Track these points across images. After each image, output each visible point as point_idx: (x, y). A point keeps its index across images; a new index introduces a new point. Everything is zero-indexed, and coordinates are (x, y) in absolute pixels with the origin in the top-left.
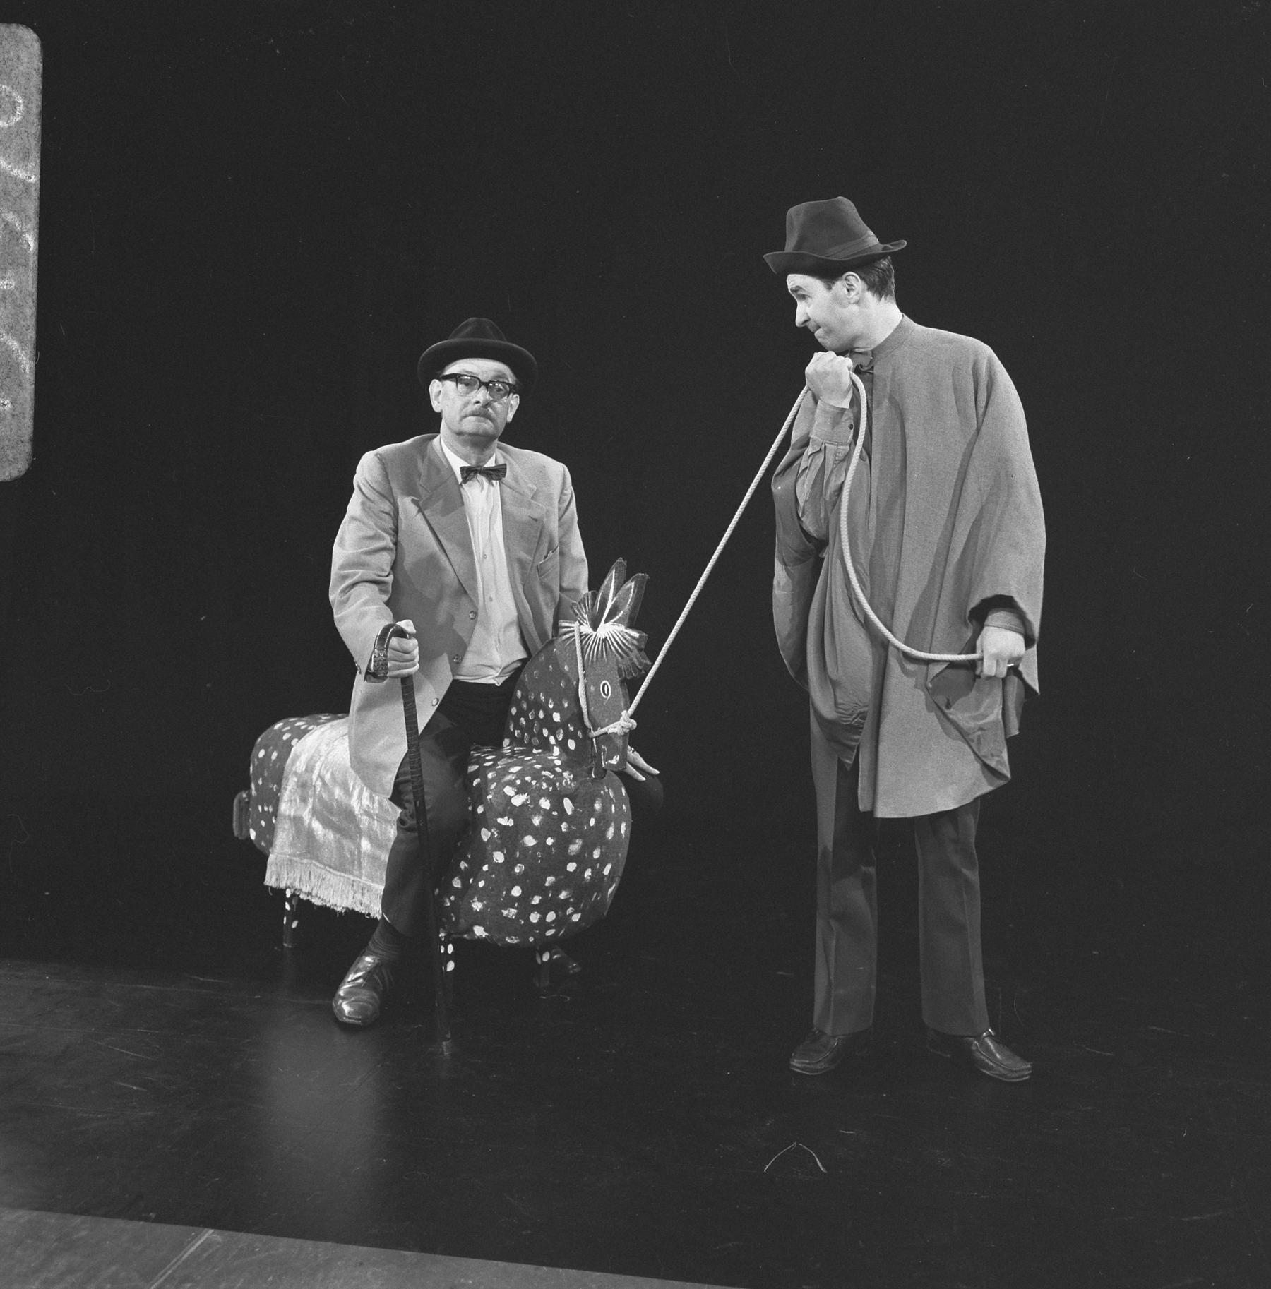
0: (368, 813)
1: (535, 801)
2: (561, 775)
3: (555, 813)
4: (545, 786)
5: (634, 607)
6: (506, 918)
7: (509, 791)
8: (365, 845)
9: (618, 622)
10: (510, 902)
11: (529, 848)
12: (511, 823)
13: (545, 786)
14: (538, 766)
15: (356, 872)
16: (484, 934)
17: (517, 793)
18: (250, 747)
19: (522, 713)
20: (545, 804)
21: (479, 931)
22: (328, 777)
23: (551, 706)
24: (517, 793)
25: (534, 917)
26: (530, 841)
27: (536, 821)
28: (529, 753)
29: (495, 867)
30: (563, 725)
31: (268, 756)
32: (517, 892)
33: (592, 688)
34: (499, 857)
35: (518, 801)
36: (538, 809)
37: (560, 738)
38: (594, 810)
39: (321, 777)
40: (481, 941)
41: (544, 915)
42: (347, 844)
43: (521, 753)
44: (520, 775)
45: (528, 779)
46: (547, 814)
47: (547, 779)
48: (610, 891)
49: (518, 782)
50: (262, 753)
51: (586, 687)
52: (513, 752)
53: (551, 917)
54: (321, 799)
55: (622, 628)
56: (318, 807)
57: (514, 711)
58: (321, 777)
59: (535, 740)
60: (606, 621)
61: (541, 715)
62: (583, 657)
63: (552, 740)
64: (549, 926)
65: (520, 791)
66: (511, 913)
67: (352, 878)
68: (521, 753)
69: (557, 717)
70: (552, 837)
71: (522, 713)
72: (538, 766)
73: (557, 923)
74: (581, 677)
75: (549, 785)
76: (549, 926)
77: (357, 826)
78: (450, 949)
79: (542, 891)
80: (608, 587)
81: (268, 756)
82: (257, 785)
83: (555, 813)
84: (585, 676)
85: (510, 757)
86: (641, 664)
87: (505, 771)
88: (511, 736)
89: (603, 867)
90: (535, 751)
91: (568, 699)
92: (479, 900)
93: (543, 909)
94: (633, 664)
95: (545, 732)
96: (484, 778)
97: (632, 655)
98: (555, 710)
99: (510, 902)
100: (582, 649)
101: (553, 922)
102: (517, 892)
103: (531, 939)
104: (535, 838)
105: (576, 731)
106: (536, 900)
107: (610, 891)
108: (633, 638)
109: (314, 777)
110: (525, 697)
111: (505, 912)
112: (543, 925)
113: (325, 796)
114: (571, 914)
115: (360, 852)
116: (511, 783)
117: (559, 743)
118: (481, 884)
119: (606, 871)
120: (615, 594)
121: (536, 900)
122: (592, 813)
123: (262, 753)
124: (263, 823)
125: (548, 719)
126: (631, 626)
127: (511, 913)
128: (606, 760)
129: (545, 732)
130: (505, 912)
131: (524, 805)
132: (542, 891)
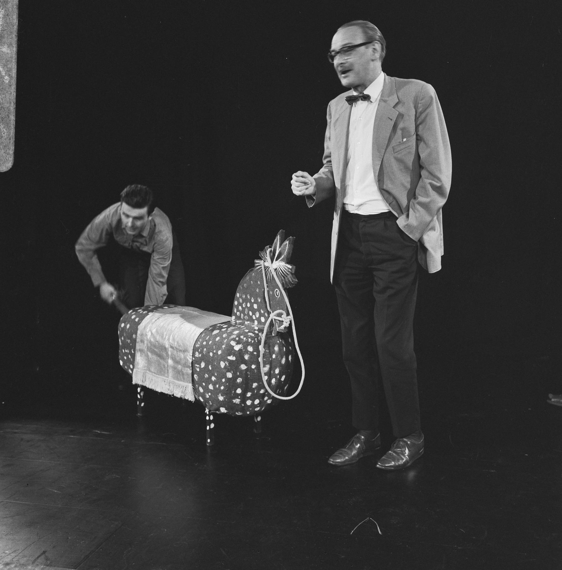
0: (172, 347)
1: (245, 347)
2: (258, 334)
3: (255, 353)
4: (250, 340)
5: (288, 253)
6: (235, 403)
7: (233, 343)
8: (170, 362)
9: (281, 260)
10: (236, 396)
11: (243, 370)
12: (234, 358)
13: (250, 340)
14: (247, 331)
15: (166, 375)
16: (226, 411)
17: (237, 344)
18: (118, 322)
19: (240, 304)
20: (250, 349)
21: (223, 410)
22: (154, 331)
23: (253, 301)
24: (237, 344)
25: (249, 403)
26: (243, 367)
27: (246, 357)
28: (242, 324)
29: (228, 380)
30: (258, 310)
31: (125, 326)
32: (239, 391)
33: (271, 293)
34: (229, 375)
35: (237, 348)
36: (247, 352)
37: (257, 316)
38: (274, 350)
39: (151, 331)
40: (223, 414)
41: (253, 401)
42: (162, 361)
43: (240, 324)
44: (238, 335)
45: (242, 337)
46: (251, 353)
47: (251, 337)
48: (286, 388)
49: (237, 339)
50: (123, 325)
51: (268, 291)
52: (236, 324)
53: (257, 402)
54: (150, 342)
55: (283, 264)
56: (149, 345)
57: (236, 303)
58: (151, 331)
59: (246, 317)
60: (276, 260)
61: (249, 305)
62: (266, 278)
63: (254, 318)
64: (256, 406)
65: (238, 343)
66: (237, 401)
67: (164, 378)
68: (240, 324)
69: (255, 306)
70: (255, 364)
71: (240, 304)
72: (247, 331)
73: (260, 404)
74: (266, 287)
75: (252, 340)
76: (256, 406)
77: (167, 353)
78: (212, 418)
79: (252, 390)
80: (276, 244)
81: (125, 326)
82: (121, 340)
83: (255, 353)
84: (267, 287)
85: (234, 326)
86: (293, 281)
87: (231, 333)
88: (236, 315)
89: (281, 377)
90: (246, 323)
91: (260, 297)
92: (222, 396)
93: (253, 398)
94: (289, 281)
95: (251, 313)
96: (221, 337)
97: (288, 276)
98: (254, 303)
99: (236, 396)
100: (266, 273)
101: (258, 404)
102: (239, 391)
103: (248, 413)
104: (246, 365)
105: (264, 313)
106: (249, 394)
107: (286, 388)
108: (289, 268)
109: (148, 330)
110: (241, 297)
111: (234, 401)
112: (253, 406)
113: (152, 340)
114: (267, 400)
115: (168, 366)
116: (234, 339)
117: (257, 319)
118: (222, 388)
119: (283, 379)
120: (280, 247)
121: (249, 394)
122: (274, 352)
123: (123, 325)
124: (125, 358)
125: (251, 309)
126: (288, 262)
127: (237, 401)
128: (279, 326)
129: (251, 313)
130: (234, 401)
131: (240, 350)
132: (252, 390)
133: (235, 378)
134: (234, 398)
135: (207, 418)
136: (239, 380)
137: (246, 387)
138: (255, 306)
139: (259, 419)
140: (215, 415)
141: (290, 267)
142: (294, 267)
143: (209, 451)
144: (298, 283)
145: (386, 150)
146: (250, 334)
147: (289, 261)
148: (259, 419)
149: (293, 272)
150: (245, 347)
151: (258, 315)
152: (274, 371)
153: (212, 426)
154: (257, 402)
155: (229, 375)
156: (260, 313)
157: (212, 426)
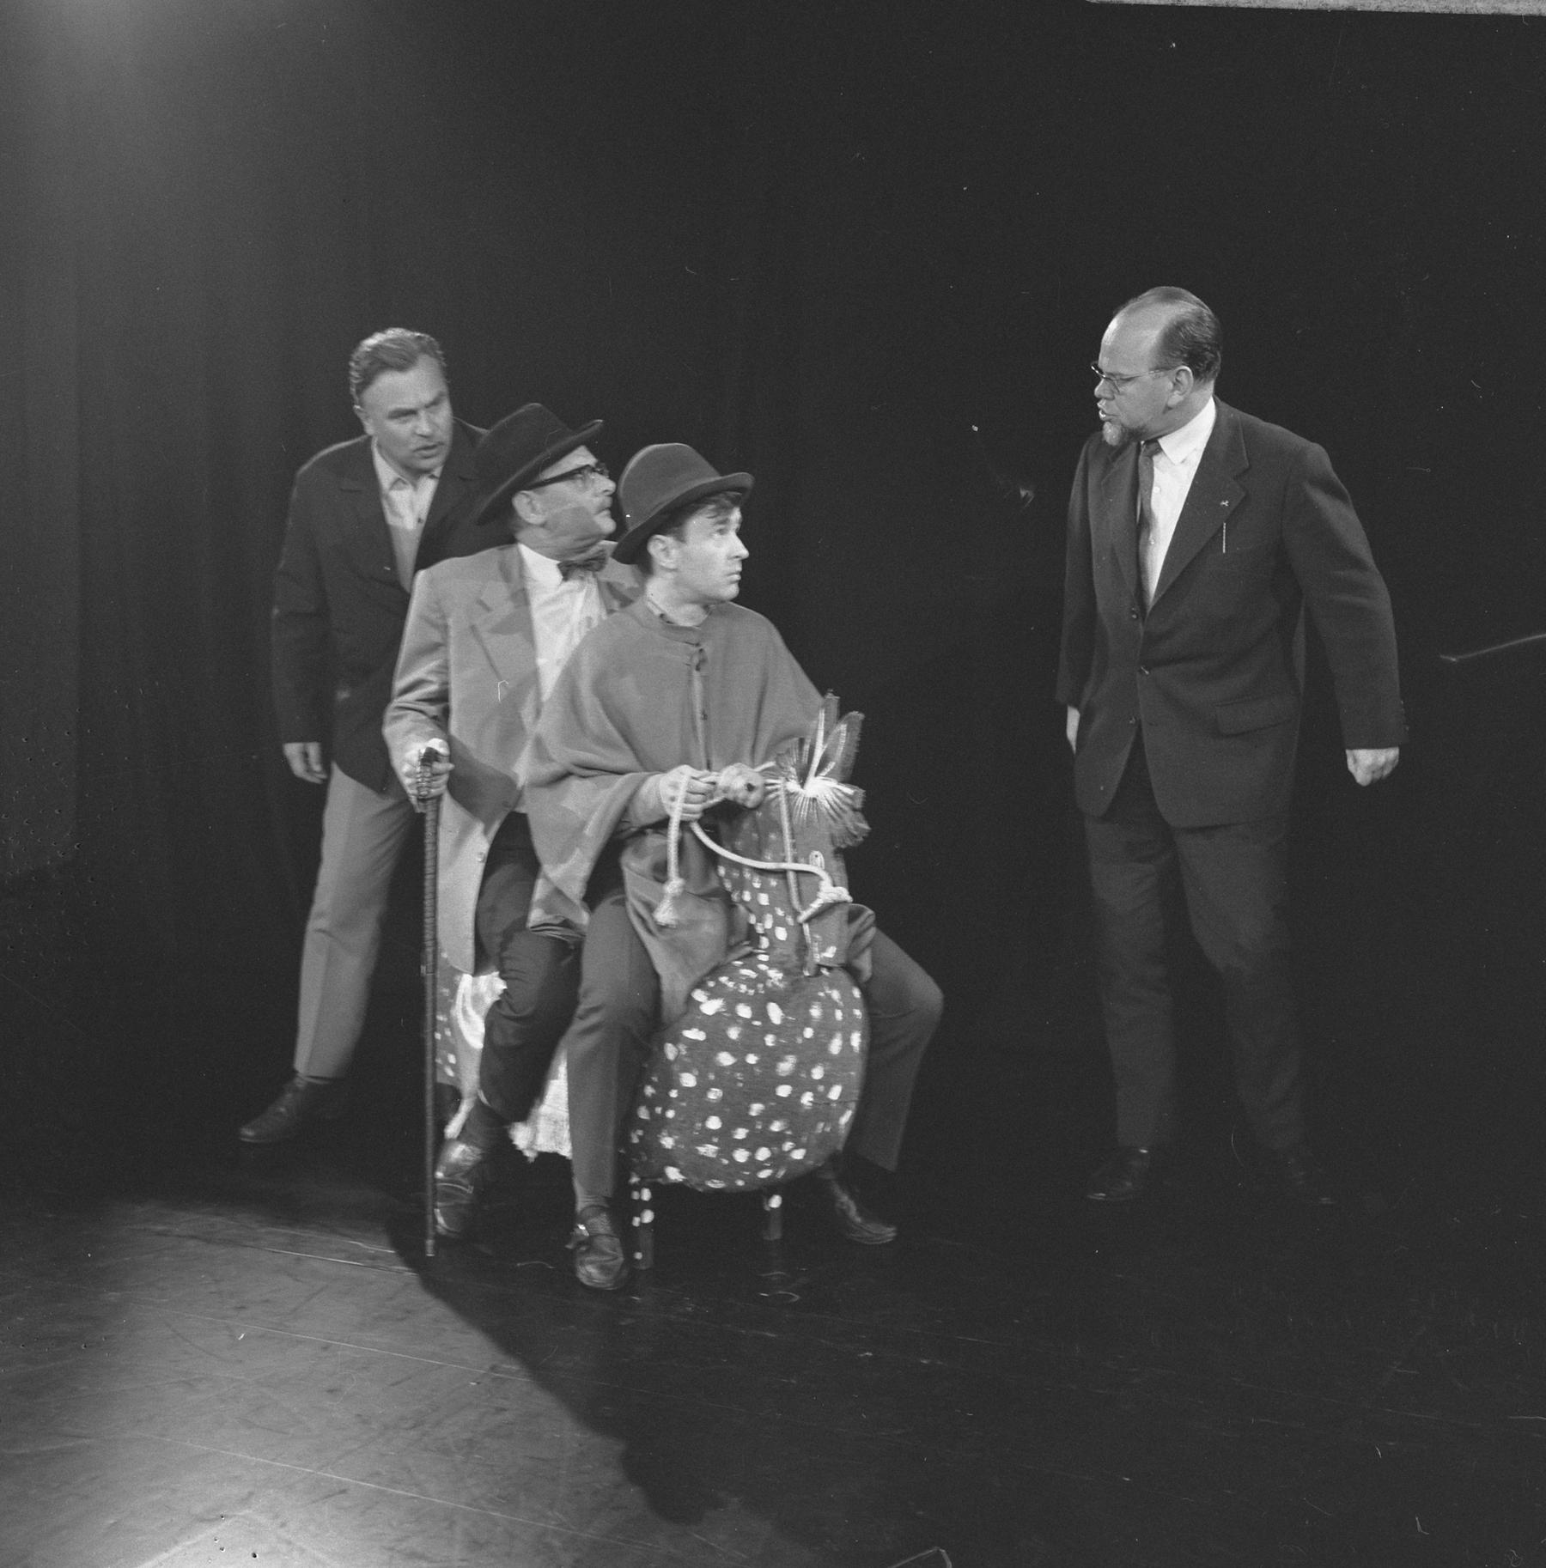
1: (761, 1013)
3: (757, 1023)
5: (846, 755)
6: (703, 1157)
9: (830, 775)
10: (707, 1136)
17: (710, 998)
20: (744, 1011)
26: (726, 1059)
36: (735, 1019)
46: (747, 1023)
47: (748, 981)
53: (763, 1154)
55: (833, 783)
66: (709, 1150)
79: (747, 1122)
83: (757, 1023)
84: (794, 846)
93: (751, 1144)
98: (762, 890)
99: (707, 1136)
101: (767, 1160)
108: (846, 795)
111: (702, 1150)
121: (741, 1134)
126: (848, 780)
127: (709, 1150)
130: (702, 1150)
132: (747, 1122)
133: (703, 1087)
134: (702, 1142)
135: (635, 1195)
136: (714, 1094)
137: (734, 1114)
138: (764, 899)
139: (776, 1202)
140: (654, 1188)
141: (849, 790)
142: (861, 792)
143: (285, 1106)
144: (870, 833)
145: (489, 658)
146: (745, 972)
147: (851, 776)
148: (776, 1202)
149: (858, 805)
150: (731, 1006)
151: (769, 924)
152: (809, 1073)
153: (648, 1217)
154: (763, 1154)
155: (688, 1080)
156: (776, 917)
157: (648, 1217)
